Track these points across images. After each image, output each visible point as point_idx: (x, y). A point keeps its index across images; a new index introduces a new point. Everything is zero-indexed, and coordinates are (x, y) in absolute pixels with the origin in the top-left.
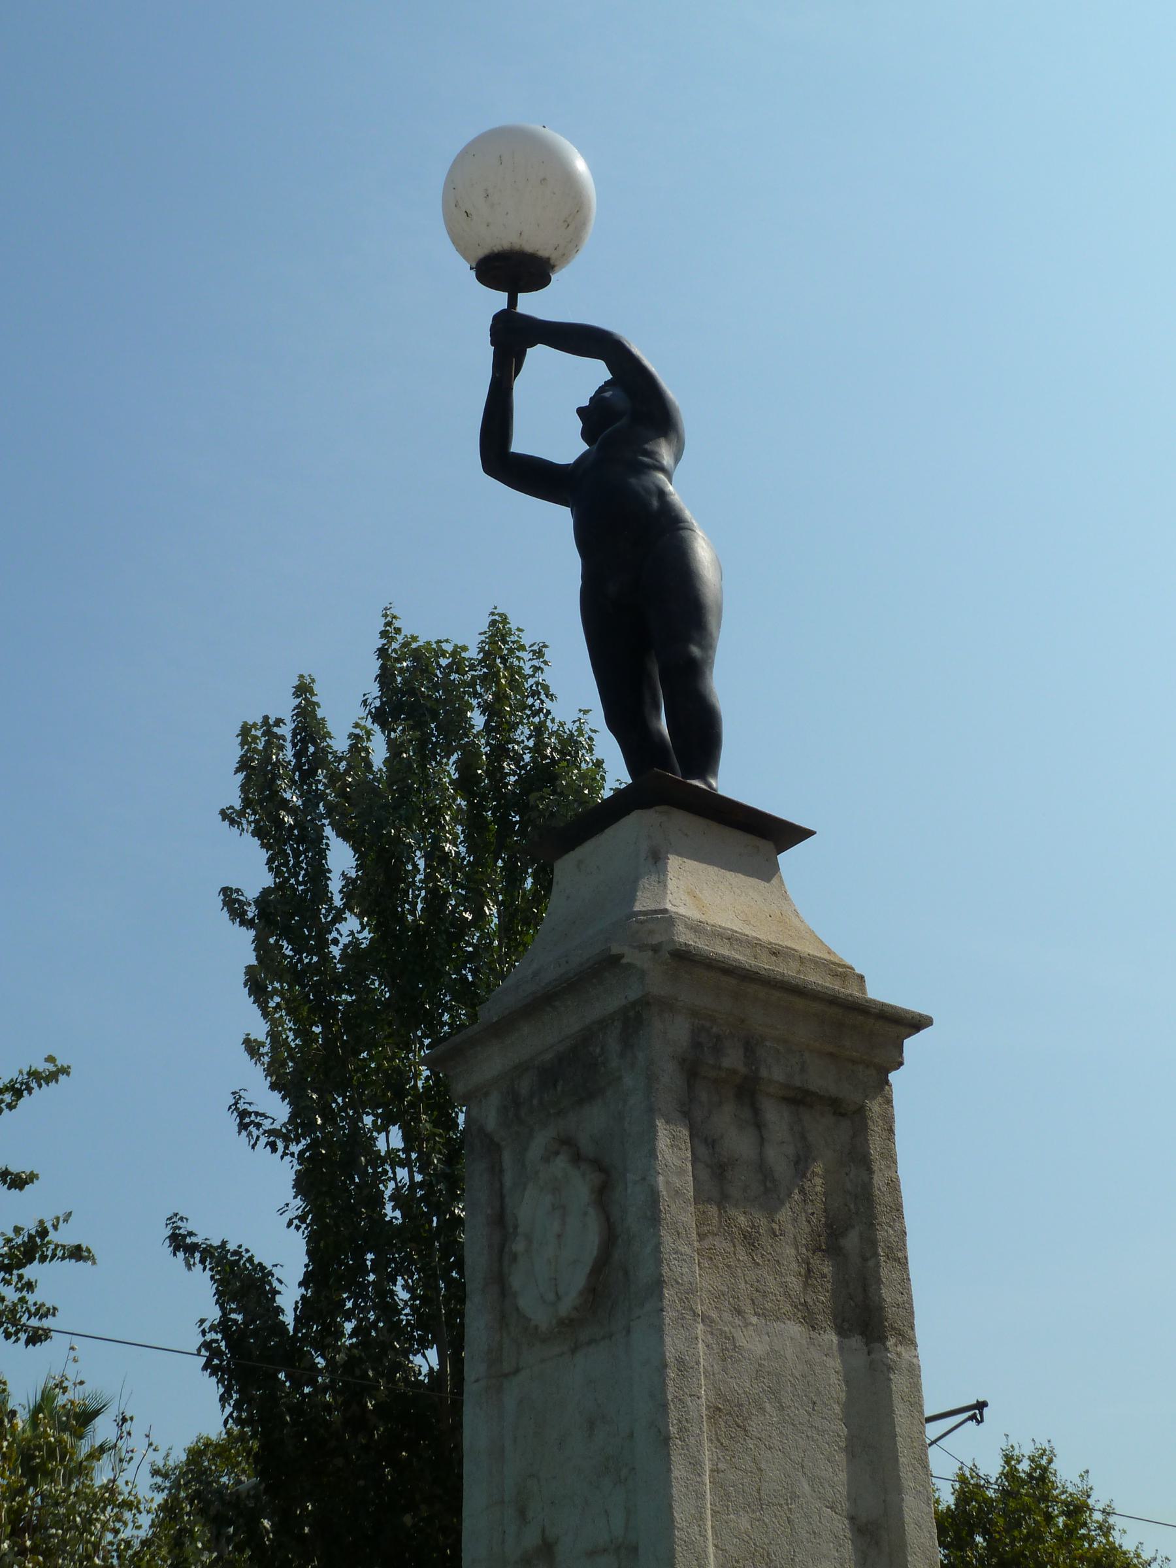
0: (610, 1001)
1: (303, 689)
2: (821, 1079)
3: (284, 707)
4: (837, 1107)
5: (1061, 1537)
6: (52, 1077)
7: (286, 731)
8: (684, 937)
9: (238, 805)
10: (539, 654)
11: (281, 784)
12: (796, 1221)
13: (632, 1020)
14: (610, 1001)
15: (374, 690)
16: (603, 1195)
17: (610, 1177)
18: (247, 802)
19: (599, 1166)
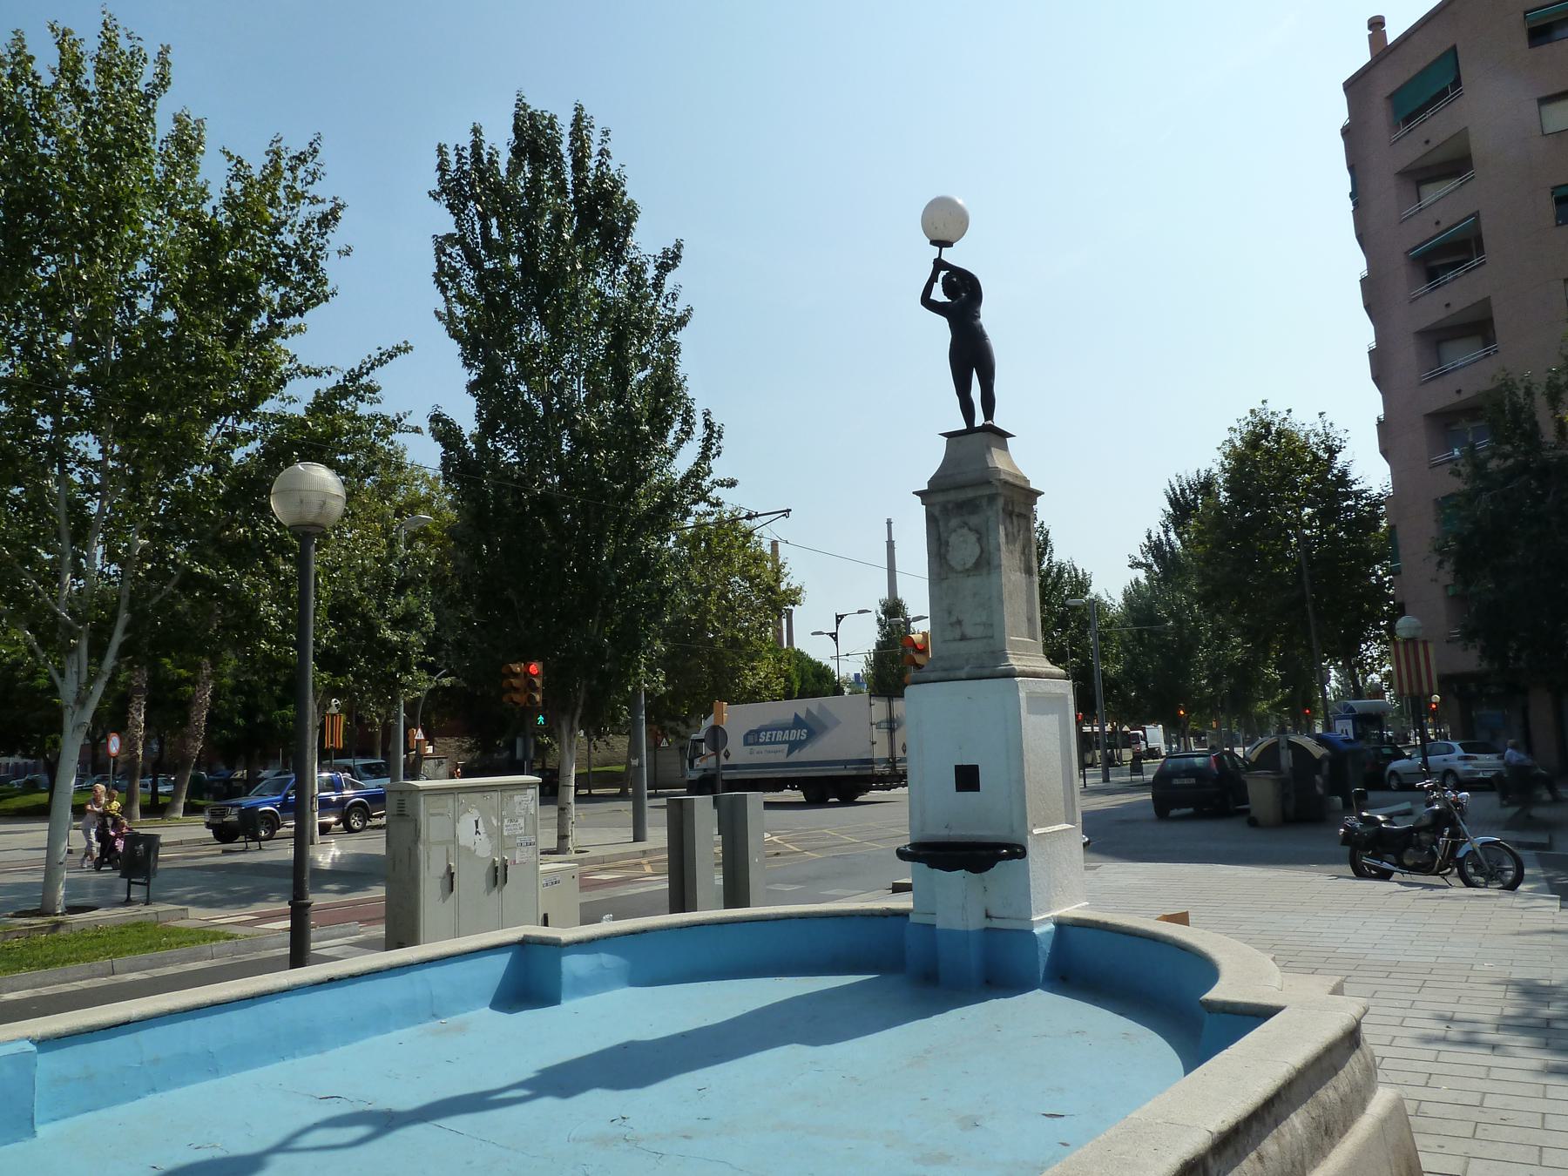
0: (986, 491)
1: (476, 131)
2: (1023, 511)
3: (466, 141)
4: (1020, 515)
5: (24, 262)
6: (406, 351)
7: (466, 154)
8: (1003, 476)
9: (438, 189)
10: (606, 133)
11: (466, 182)
12: (1018, 547)
13: (992, 499)
14: (986, 491)
15: (513, 136)
16: (979, 540)
17: (982, 535)
18: (444, 190)
19: (977, 532)
